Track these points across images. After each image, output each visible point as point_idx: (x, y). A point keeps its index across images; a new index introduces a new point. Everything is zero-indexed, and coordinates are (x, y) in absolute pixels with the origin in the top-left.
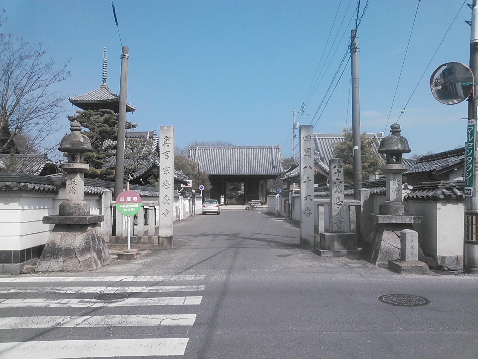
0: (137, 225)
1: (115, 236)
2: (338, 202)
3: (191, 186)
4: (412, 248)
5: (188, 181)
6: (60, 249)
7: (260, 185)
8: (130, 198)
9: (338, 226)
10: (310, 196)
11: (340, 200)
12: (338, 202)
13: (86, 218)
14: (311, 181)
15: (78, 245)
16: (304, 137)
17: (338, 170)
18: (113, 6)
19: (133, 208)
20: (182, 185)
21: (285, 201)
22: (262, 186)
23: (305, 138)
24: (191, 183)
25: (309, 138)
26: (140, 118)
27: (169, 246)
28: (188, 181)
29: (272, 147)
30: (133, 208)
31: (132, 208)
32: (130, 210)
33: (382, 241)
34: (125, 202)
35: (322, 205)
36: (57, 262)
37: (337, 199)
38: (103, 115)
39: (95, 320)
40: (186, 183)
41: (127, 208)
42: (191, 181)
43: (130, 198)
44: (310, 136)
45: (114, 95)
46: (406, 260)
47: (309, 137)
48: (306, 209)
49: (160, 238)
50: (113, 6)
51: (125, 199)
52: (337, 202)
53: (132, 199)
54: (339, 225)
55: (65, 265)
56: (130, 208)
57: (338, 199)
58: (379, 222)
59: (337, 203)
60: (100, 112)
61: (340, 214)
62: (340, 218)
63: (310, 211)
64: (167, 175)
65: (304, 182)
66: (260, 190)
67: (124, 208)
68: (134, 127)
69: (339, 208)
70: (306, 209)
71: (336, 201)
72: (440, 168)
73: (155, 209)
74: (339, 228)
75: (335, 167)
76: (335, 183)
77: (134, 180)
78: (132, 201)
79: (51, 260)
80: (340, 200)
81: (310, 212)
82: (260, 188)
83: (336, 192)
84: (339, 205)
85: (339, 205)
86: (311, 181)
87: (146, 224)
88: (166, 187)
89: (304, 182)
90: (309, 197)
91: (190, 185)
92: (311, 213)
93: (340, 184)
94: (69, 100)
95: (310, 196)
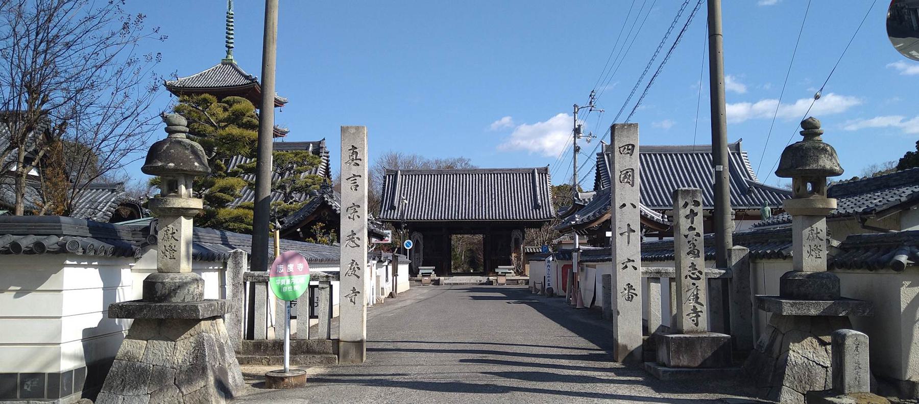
0: (295, 318)
1: (253, 338)
3: (390, 242)
4: (858, 366)
7: (513, 240)
17: (692, 211)
18: (229, 17)
21: (565, 268)
26: (292, 120)
27: (359, 360)
29: (534, 171)
33: (791, 352)
35: (657, 280)
36: (138, 396)
38: (224, 121)
42: (390, 232)
44: (633, 146)
45: (247, 77)
46: (846, 392)
49: (341, 344)
50: (229, 17)
58: (784, 314)
60: (225, 102)
64: (356, 223)
65: (621, 234)
68: (283, 133)
69: (694, 284)
72: (885, 207)
73: (331, 287)
75: (686, 205)
76: (686, 236)
79: (124, 393)
87: (312, 316)
89: (621, 234)
90: (631, 263)
91: (389, 240)
94: (165, 85)
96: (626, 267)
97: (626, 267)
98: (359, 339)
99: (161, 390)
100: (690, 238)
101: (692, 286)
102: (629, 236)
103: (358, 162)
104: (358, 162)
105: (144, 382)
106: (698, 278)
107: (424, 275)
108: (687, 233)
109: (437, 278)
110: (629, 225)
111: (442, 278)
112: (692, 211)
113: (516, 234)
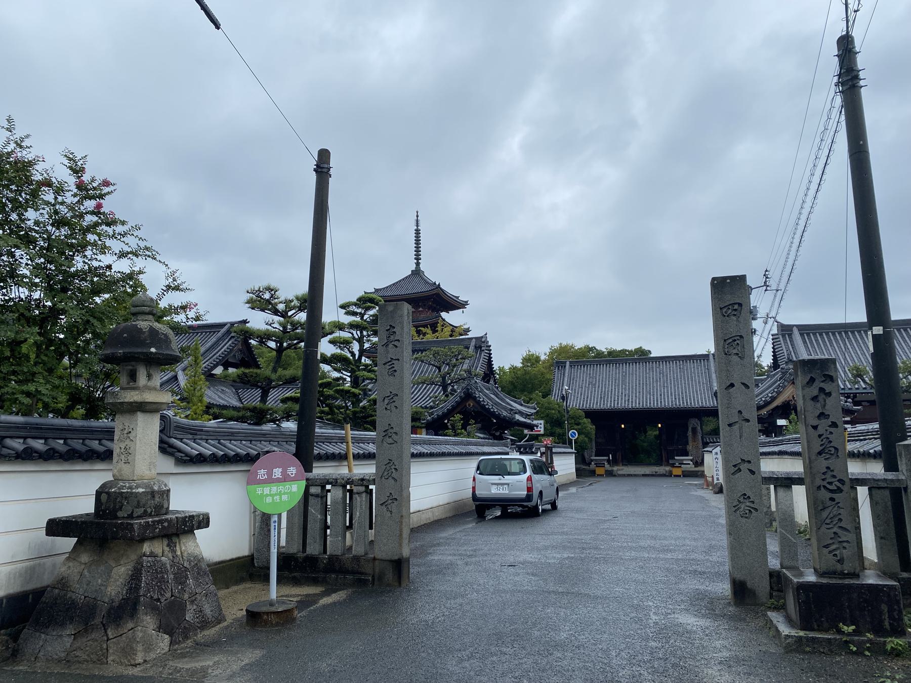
2: (830, 483)
5: (535, 422)
6: (73, 604)
7: (690, 429)
8: (280, 470)
9: (835, 555)
10: (749, 462)
11: (834, 477)
12: (830, 483)
13: (132, 525)
14: (748, 421)
15: (113, 594)
16: (721, 309)
19: (286, 493)
20: (526, 432)
22: (694, 431)
23: (725, 310)
24: (542, 426)
25: (736, 310)
28: (535, 422)
30: (286, 493)
31: (284, 493)
32: (281, 498)
34: (270, 480)
37: (824, 474)
39: (776, 449)
40: (531, 427)
41: (272, 496)
42: (542, 422)
43: (280, 470)
47: (736, 307)
48: (741, 499)
51: (270, 474)
52: (825, 483)
53: (284, 473)
54: (837, 552)
55: (77, 644)
56: (280, 494)
57: (828, 476)
59: (828, 486)
61: (840, 520)
62: (840, 532)
63: (753, 502)
66: (690, 439)
67: (267, 495)
69: (832, 499)
70: (741, 499)
71: (823, 480)
74: (838, 561)
77: (434, 420)
78: (285, 479)
80: (834, 477)
81: (752, 505)
82: (690, 433)
83: (820, 453)
84: (832, 491)
85: (832, 491)
86: (748, 421)
88: (390, 441)
92: (756, 510)
93: (832, 430)
95: (749, 462)
96: (739, 470)
97: (739, 470)
98: (396, 558)
99: (86, 630)
100: (821, 430)
101: (829, 503)
102: (741, 428)
103: (396, 343)
104: (396, 343)
105: (71, 619)
106: (839, 490)
107: (598, 465)
108: (815, 422)
109: (610, 469)
110: (740, 412)
111: (615, 468)
112: (822, 390)
113: (693, 422)
